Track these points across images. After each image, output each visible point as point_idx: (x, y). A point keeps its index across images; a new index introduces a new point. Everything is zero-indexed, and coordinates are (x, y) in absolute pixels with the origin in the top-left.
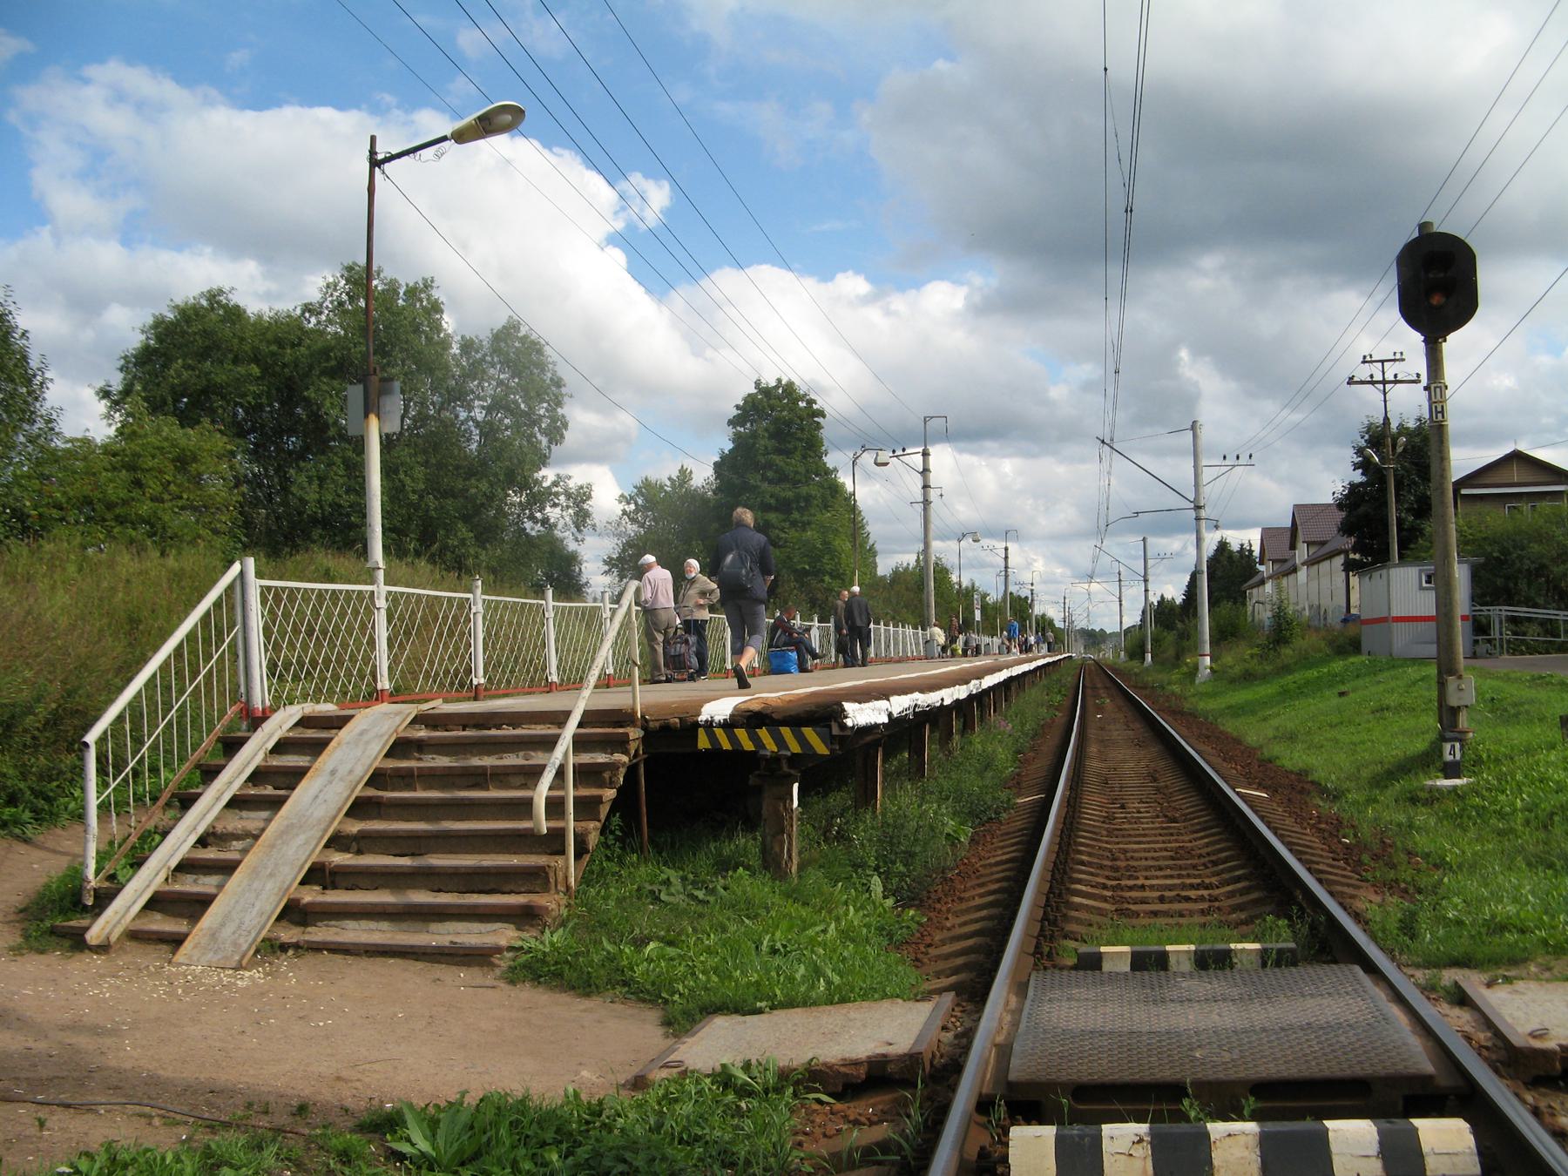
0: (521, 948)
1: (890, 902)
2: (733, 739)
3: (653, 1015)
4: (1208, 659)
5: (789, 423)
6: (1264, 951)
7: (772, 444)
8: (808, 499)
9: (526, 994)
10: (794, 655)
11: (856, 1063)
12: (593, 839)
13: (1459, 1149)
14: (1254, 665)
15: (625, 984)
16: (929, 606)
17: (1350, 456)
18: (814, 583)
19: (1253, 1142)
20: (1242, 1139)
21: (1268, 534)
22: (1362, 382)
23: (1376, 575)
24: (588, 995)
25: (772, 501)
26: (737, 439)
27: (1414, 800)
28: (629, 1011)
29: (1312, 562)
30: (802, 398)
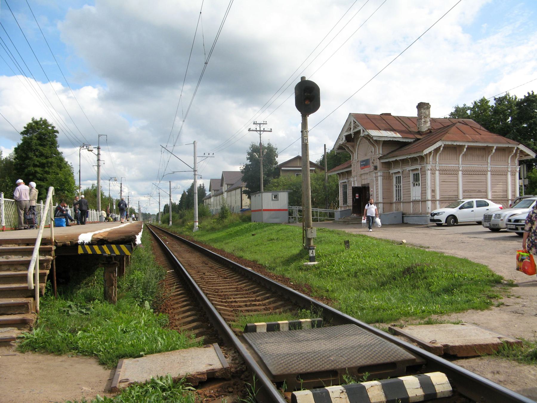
0: (23, 337)
1: (152, 310)
2: (92, 249)
3: (92, 361)
4: (197, 223)
5: (44, 135)
6: (290, 323)
7: (38, 142)
8: (51, 163)
9: (30, 357)
10: (64, 220)
11: (203, 374)
12: (44, 291)
13: (444, 382)
14: (215, 225)
15: (74, 349)
16: (98, 203)
17: (246, 156)
18: (61, 193)
19: (380, 387)
20: (376, 387)
21: (213, 182)
22: (253, 130)
23: (257, 195)
24: (60, 355)
25: (38, 163)
26: (25, 140)
27: (301, 269)
28: (81, 360)
29: (228, 191)
30: (50, 125)
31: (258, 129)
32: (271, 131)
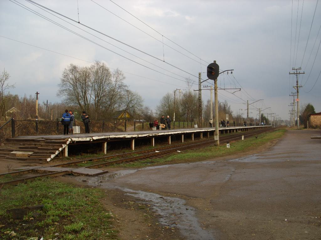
31: (296, 72)
32: (304, 73)
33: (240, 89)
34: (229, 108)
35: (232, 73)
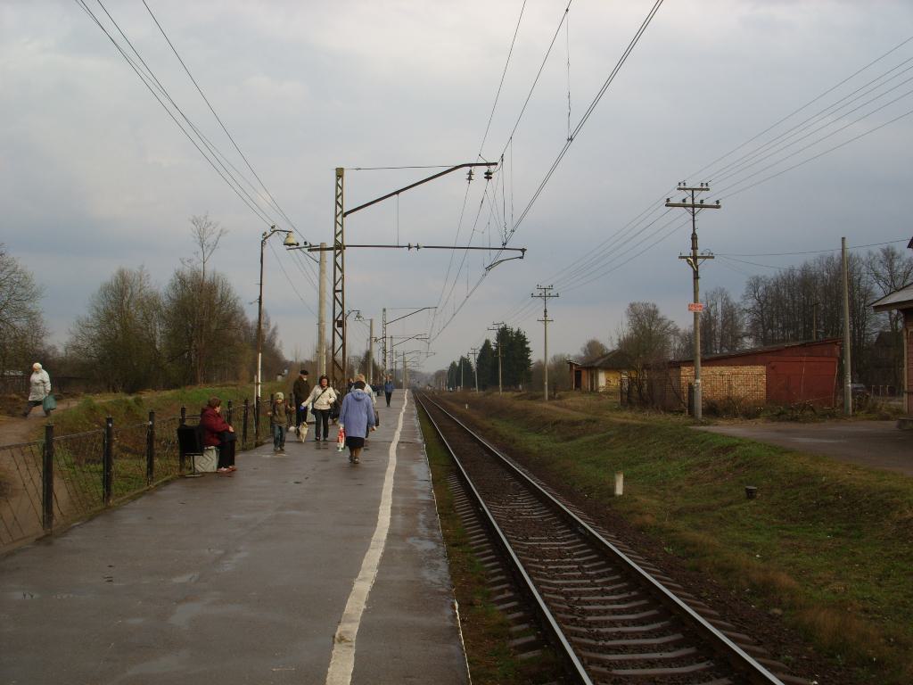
31: (689, 202)
32: (718, 207)
33: (523, 250)
34: (274, 332)
35: (488, 176)
